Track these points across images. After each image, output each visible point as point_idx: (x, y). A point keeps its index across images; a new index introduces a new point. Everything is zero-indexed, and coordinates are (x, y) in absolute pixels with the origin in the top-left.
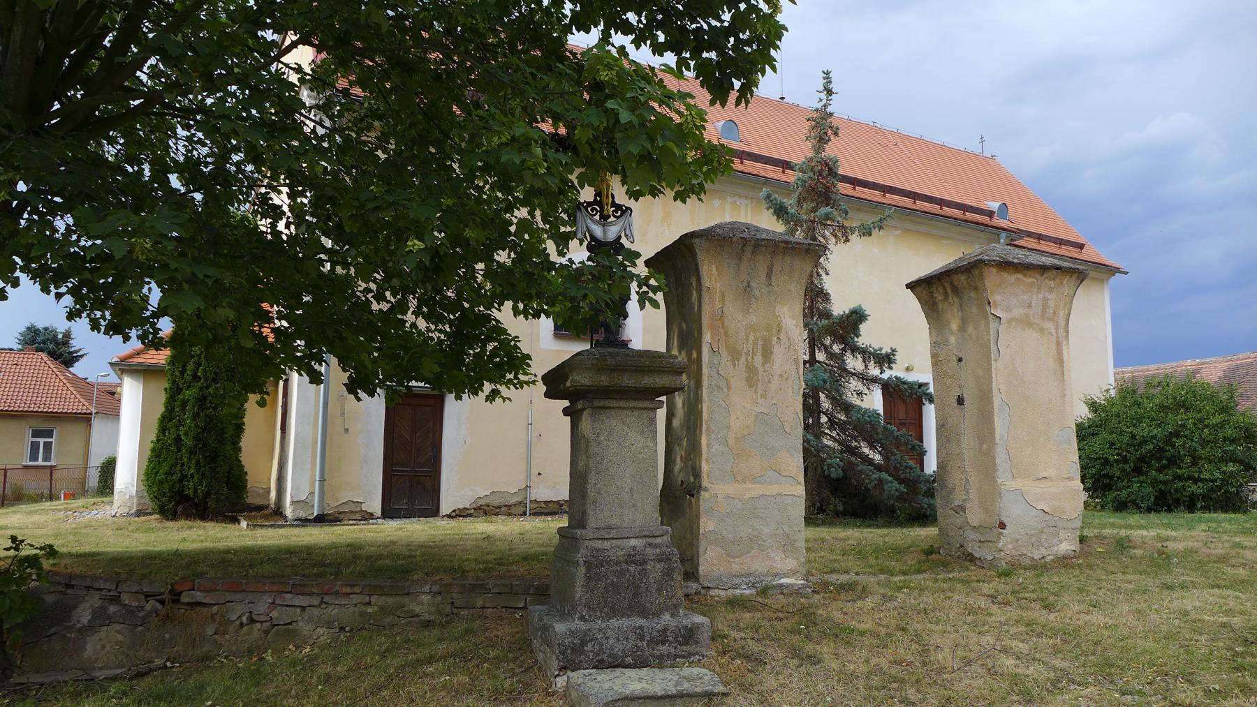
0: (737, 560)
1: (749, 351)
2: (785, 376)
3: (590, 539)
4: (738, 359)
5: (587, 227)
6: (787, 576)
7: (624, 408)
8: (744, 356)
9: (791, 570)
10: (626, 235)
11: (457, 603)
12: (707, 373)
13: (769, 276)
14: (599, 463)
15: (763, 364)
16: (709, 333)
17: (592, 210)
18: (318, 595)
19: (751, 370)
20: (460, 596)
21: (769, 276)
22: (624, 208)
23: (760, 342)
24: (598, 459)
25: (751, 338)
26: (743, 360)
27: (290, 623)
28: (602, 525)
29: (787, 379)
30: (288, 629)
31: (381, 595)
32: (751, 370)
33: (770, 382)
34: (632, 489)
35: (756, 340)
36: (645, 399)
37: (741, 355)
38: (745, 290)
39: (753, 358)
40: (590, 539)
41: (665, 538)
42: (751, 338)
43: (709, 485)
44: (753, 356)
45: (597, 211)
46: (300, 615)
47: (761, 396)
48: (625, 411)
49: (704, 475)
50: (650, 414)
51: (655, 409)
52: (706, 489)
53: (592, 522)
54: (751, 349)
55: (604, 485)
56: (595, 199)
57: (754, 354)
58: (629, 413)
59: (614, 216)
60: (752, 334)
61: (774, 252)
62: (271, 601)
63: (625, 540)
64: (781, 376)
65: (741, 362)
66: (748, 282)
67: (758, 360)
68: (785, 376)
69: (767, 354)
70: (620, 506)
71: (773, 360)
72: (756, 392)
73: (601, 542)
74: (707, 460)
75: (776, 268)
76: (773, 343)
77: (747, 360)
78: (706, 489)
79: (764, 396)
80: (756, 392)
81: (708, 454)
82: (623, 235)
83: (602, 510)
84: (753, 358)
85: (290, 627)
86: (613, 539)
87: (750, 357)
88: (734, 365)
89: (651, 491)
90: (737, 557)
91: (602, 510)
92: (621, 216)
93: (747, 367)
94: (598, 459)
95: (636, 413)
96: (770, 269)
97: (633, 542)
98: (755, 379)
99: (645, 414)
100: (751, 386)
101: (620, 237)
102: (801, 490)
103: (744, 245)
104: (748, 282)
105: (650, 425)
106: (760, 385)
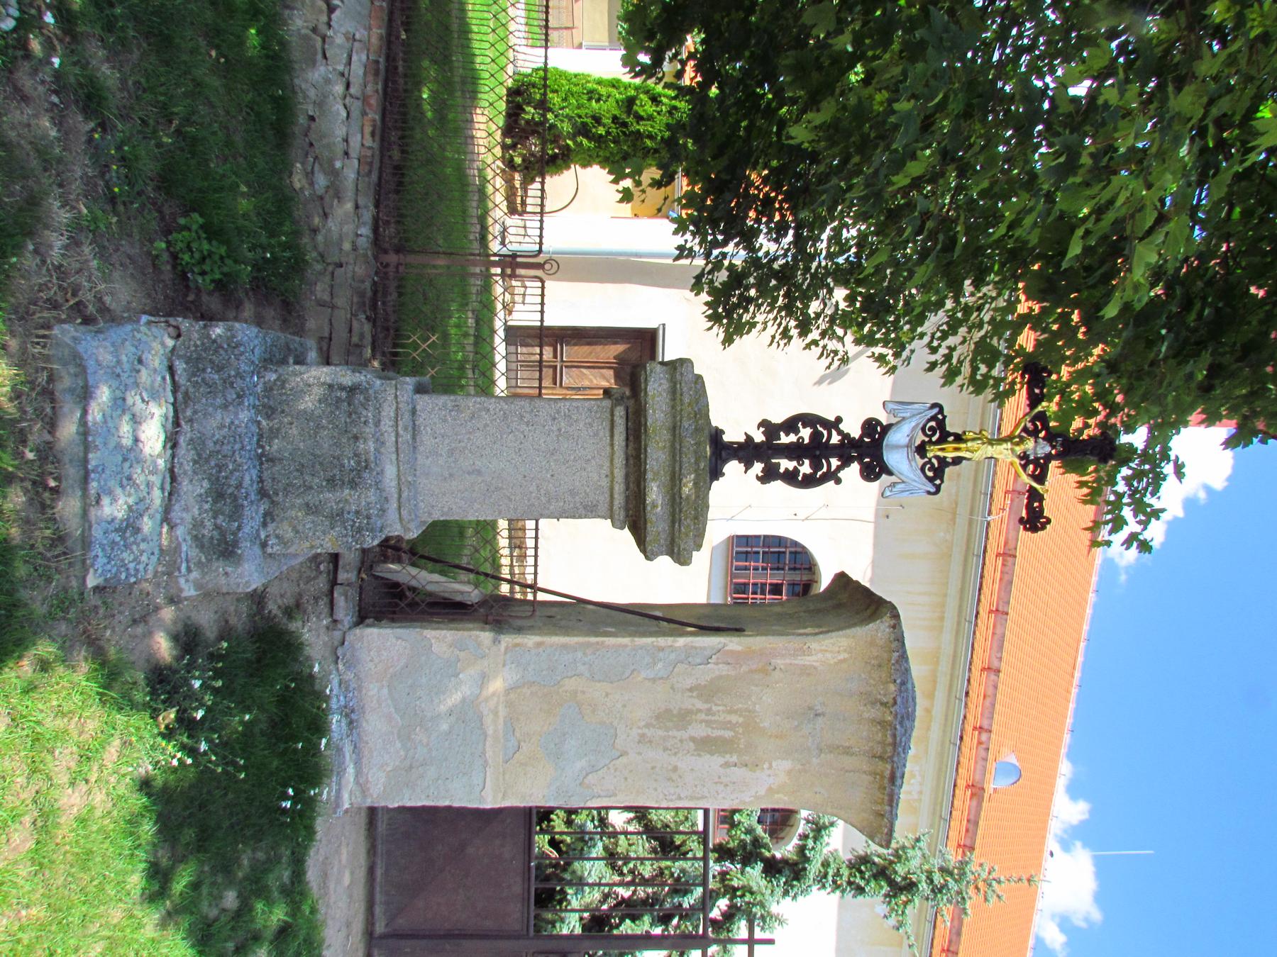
0: (385, 691)
1: (713, 715)
2: (675, 776)
3: (396, 397)
4: (700, 696)
5: (904, 419)
6: (358, 774)
7: (612, 461)
8: (706, 706)
9: (367, 781)
10: (894, 484)
11: (339, 271)
12: (677, 645)
13: (833, 749)
14: (522, 417)
15: (693, 739)
16: (739, 648)
17: (931, 428)
18: (363, 93)
19: (684, 718)
20: (349, 275)
21: (833, 749)
22: (938, 482)
23: (728, 734)
24: (527, 417)
25: (734, 718)
26: (700, 705)
27: (325, 57)
28: (419, 421)
29: (670, 779)
30: (315, 54)
31: (358, 173)
32: (684, 718)
33: (665, 749)
34: (479, 472)
35: (728, 725)
36: (627, 497)
37: (706, 702)
38: (810, 708)
39: (701, 722)
40: (396, 397)
41: (398, 526)
42: (734, 718)
43: (503, 646)
44: (706, 722)
45: (930, 436)
46: (335, 70)
47: (643, 735)
48: (608, 464)
49: (518, 639)
50: (603, 507)
51: (612, 518)
52: (496, 641)
53: (424, 401)
54: (716, 718)
55: (486, 425)
56: (950, 434)
57: (708, 723)
58: (605, 470)
59: (924, 465)
60: (741, 720)
61: (874, 756)
62: (357, 36)
63: (394, 457)
64: (675, 769)
65: (696, 701)
66: (823, 714)
67: (699, 731)
68: (675, 776)
69: (706, 745)
70: (451, 452)
71: (699, 755)
72: (648, 726)
73: (392, 414)
74: (539, 645)
75: (848, 761)
76: (728, 756)
77: (699, 711)
78: (496, 641)
79: (642, 739)
80: (648, 726)
81: (551, 646)
82: (893, 479)
83: (445, 421)
84: (701, 722)
85: (319, 56)
86: (397, 435)
87: (703, 716)
88: (691, 690)
89: (476, 506)
90: (390, 691)
91: (445, 421)
92: (927, 477)
93: (690, 712)
94: (527, 417)
95: (605, 483)
96: (847, 751)
97: (390, 471)
98: (669, 724)
99: (603, 499)
100: (658, 717)
101: (890, 473)
102: (488, 806)
103: (884, 704)
104: (823, 714)
105: (585, 508)
106: (660, 733)
